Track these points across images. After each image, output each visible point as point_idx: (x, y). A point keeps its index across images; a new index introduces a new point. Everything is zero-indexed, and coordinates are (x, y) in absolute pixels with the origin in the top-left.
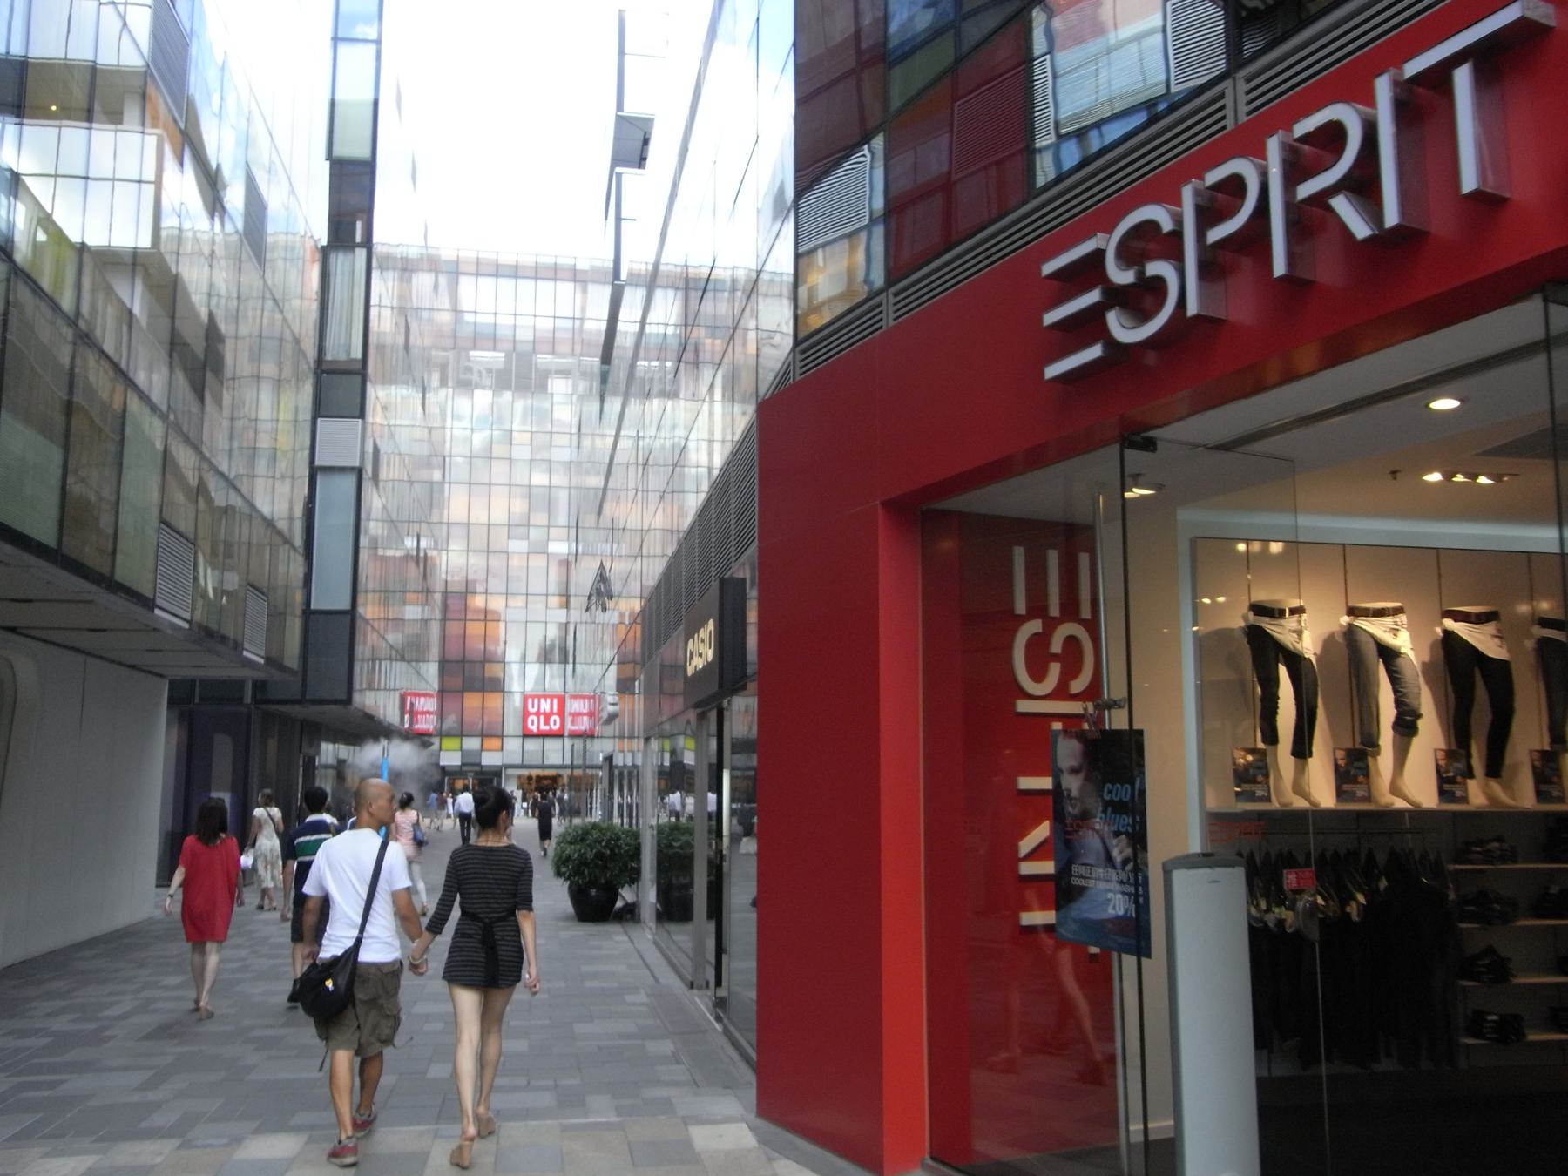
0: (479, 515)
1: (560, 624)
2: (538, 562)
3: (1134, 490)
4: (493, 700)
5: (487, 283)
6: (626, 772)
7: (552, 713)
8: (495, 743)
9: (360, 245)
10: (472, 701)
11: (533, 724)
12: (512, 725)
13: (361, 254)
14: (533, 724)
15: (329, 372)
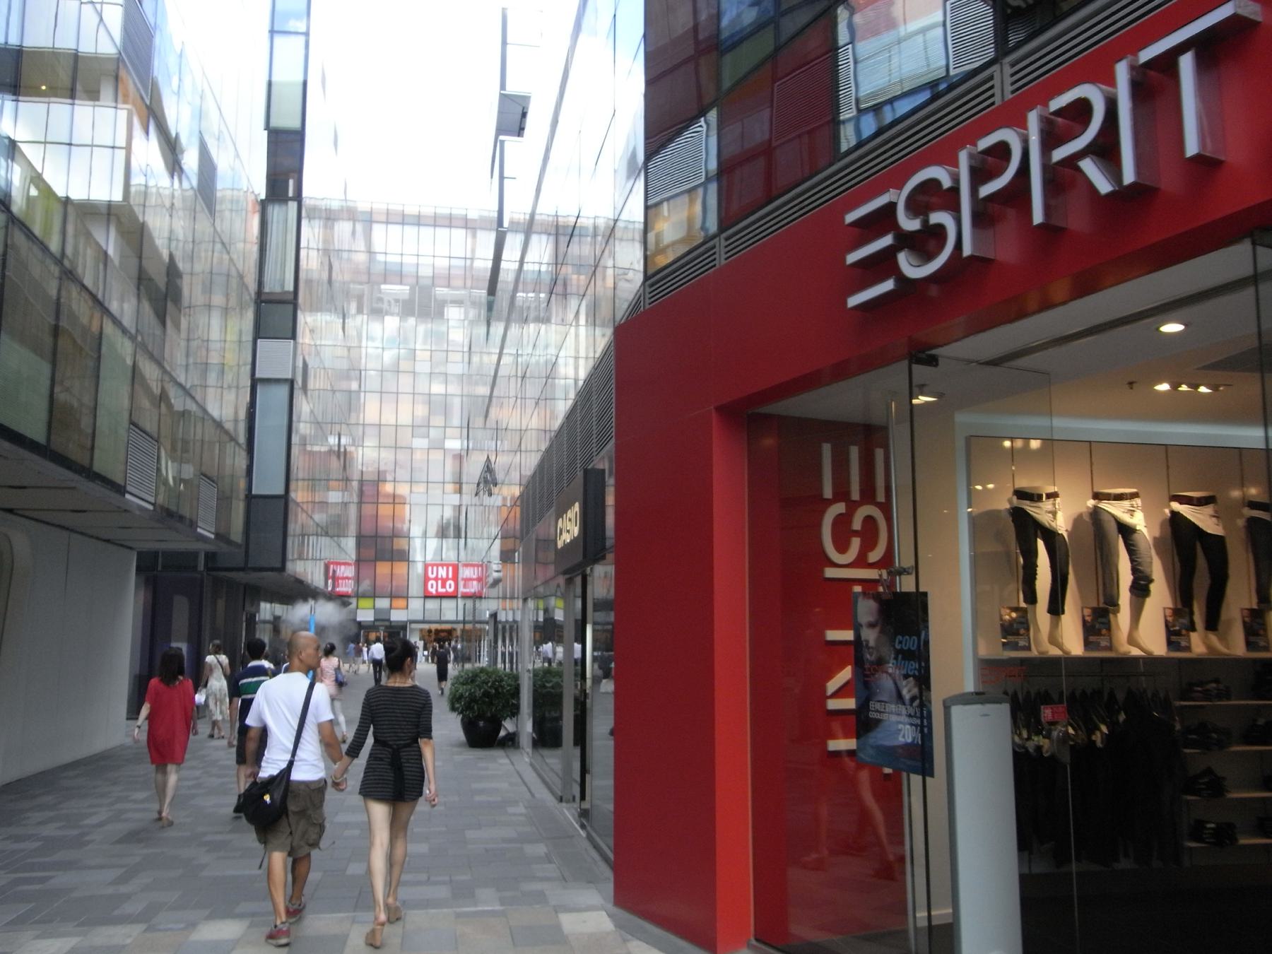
0: (388, 418)
1: (455, 506)
2: (436, 456)
4: (400, 568)
6: (507, 627)
7: (447, 579)
8: (401, 603)
9: (292, 199)
10: (383, 568)
11: (432, 587)
12: (415, 588)
13: (293, 206)
14: (432, 587)
15: (267, 302)
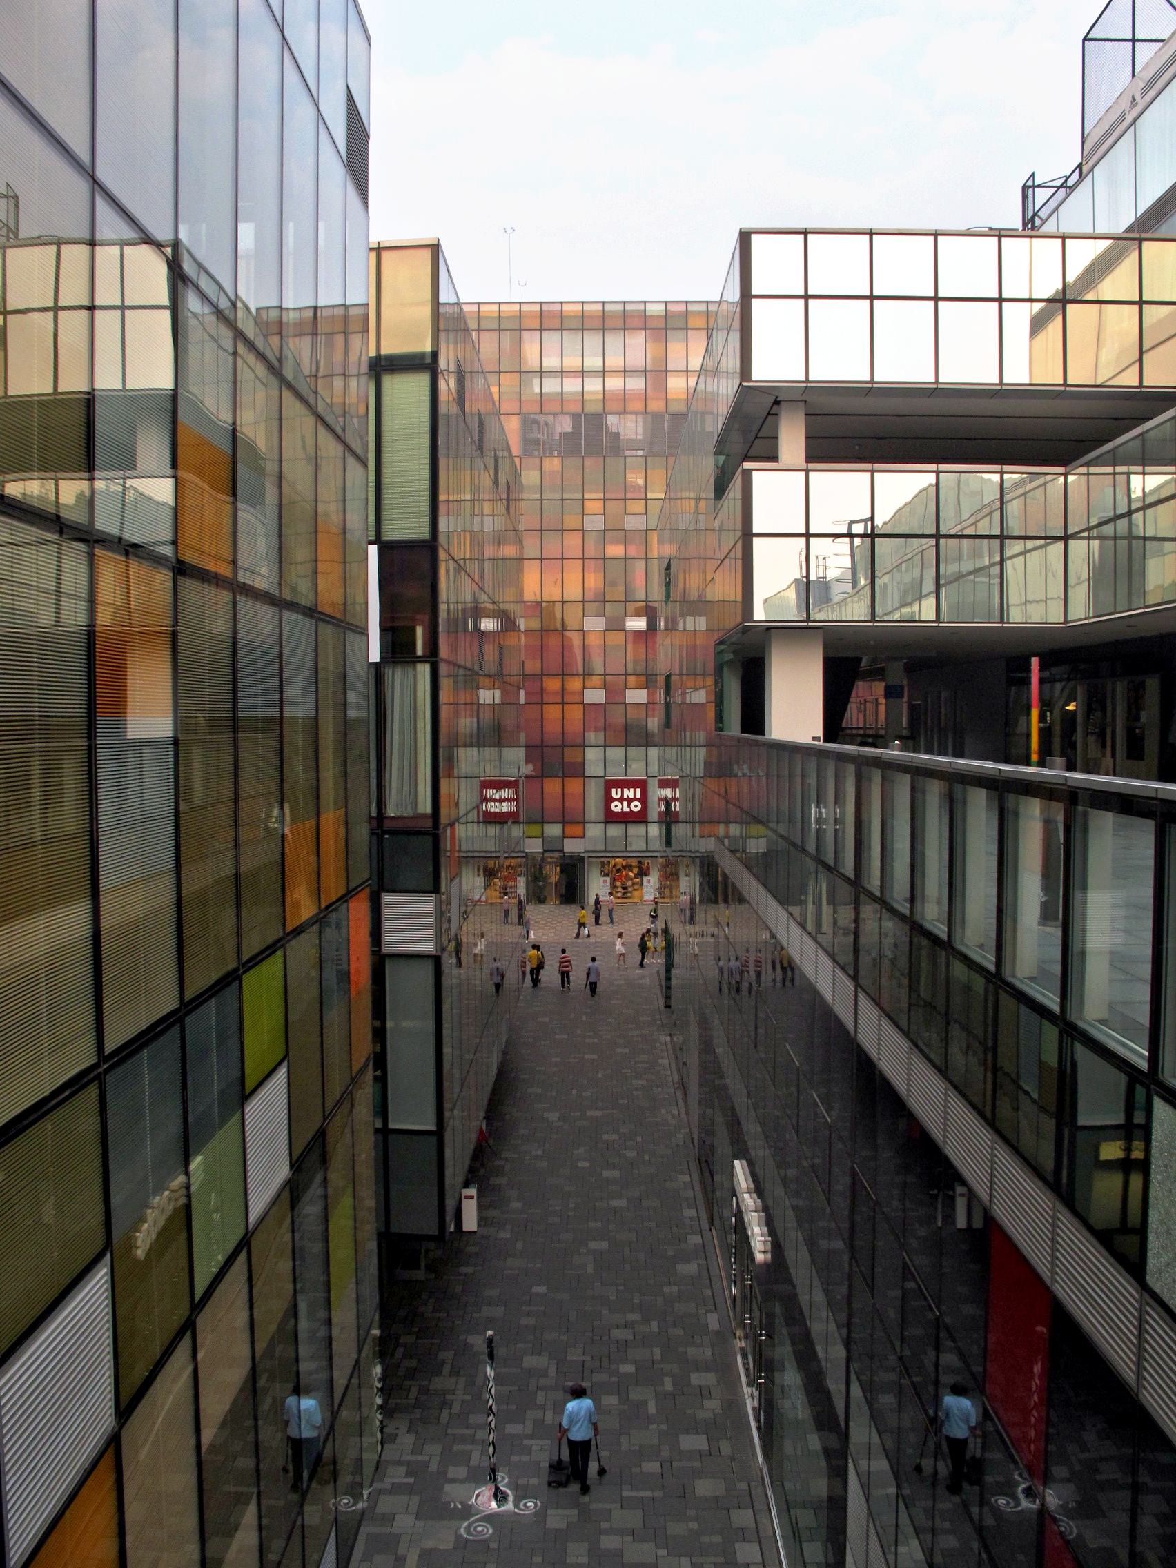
0: (552, 593)
2: (616, 639)
4: (573, 786)
5: (552, 339)
8: (577, 829)
9: (422, 660)
10: (552, 787)
12: (594, 809)
13: (424, 670)
15: (393, 832)
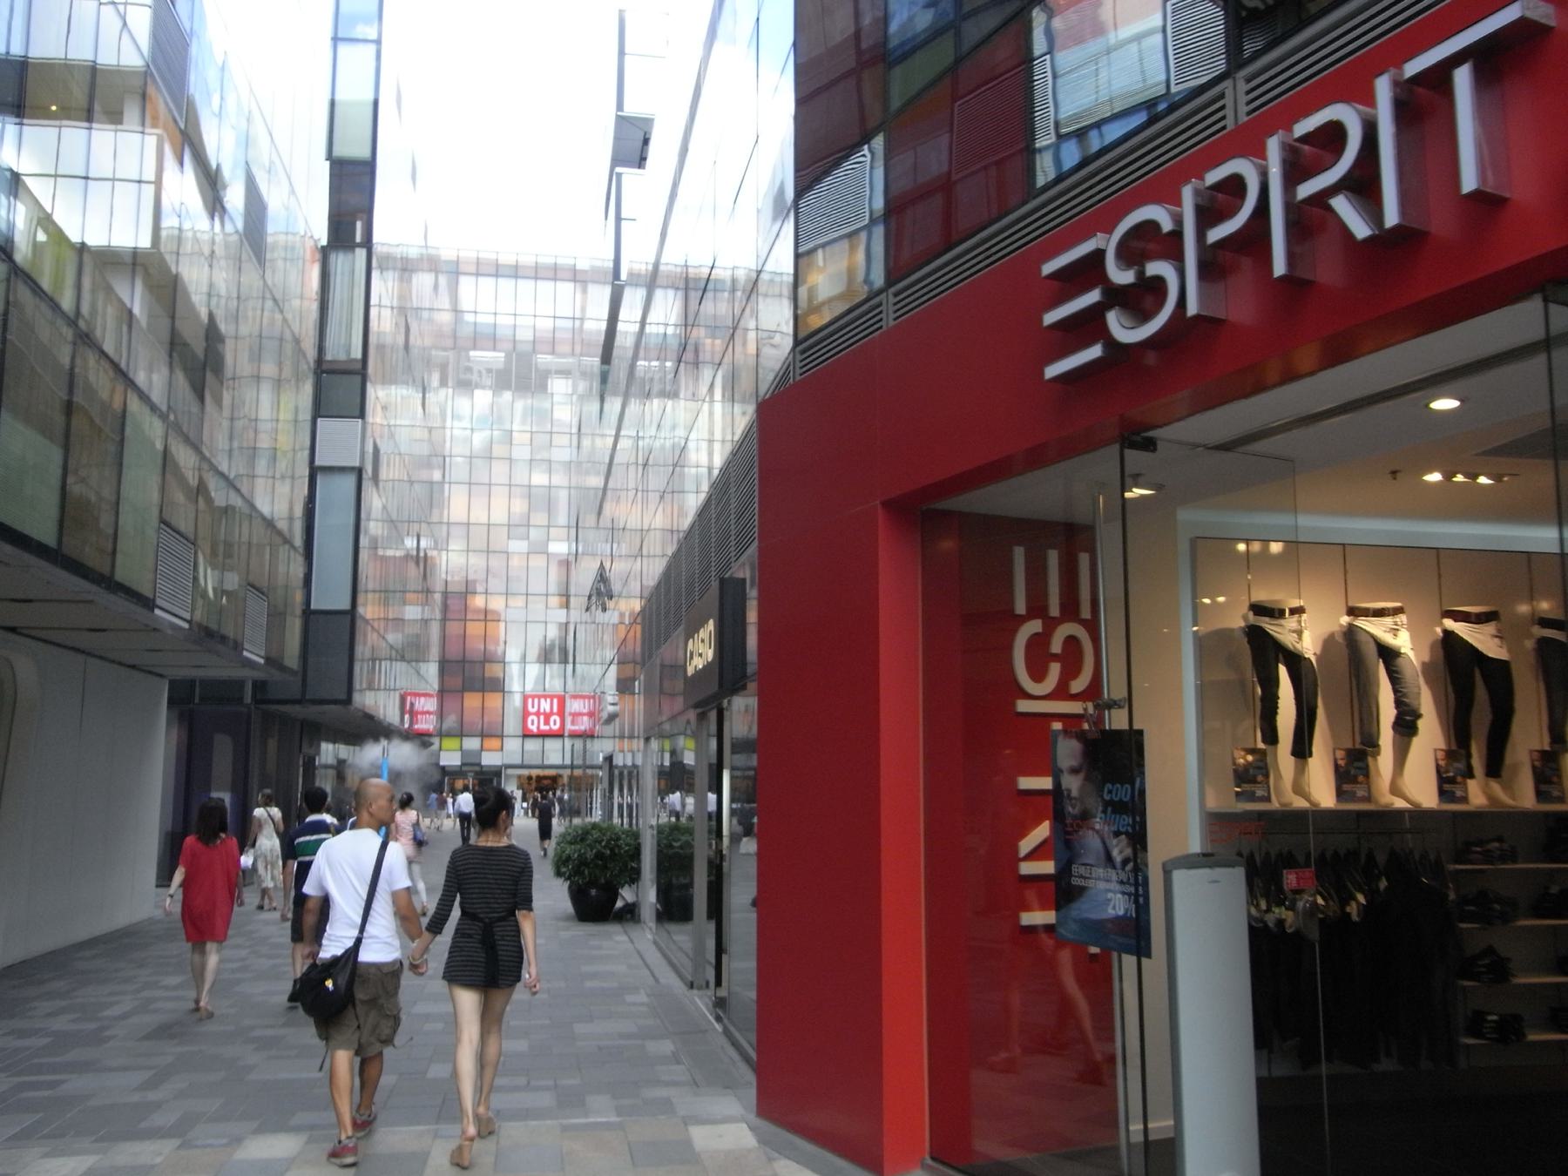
0: (479, 515)
2: (538, 562)
3: (1134, 490)
4: (493, 700)
5: (487, 283)
6: (626, 772)
7: (552, 713)
8: (495, 743)
9: (360, 245)
10: (472, 701)
11: (533, 724)
12: (512, 725)
13: (361, 254)
14: (533, 724)
15: (329, 372)
